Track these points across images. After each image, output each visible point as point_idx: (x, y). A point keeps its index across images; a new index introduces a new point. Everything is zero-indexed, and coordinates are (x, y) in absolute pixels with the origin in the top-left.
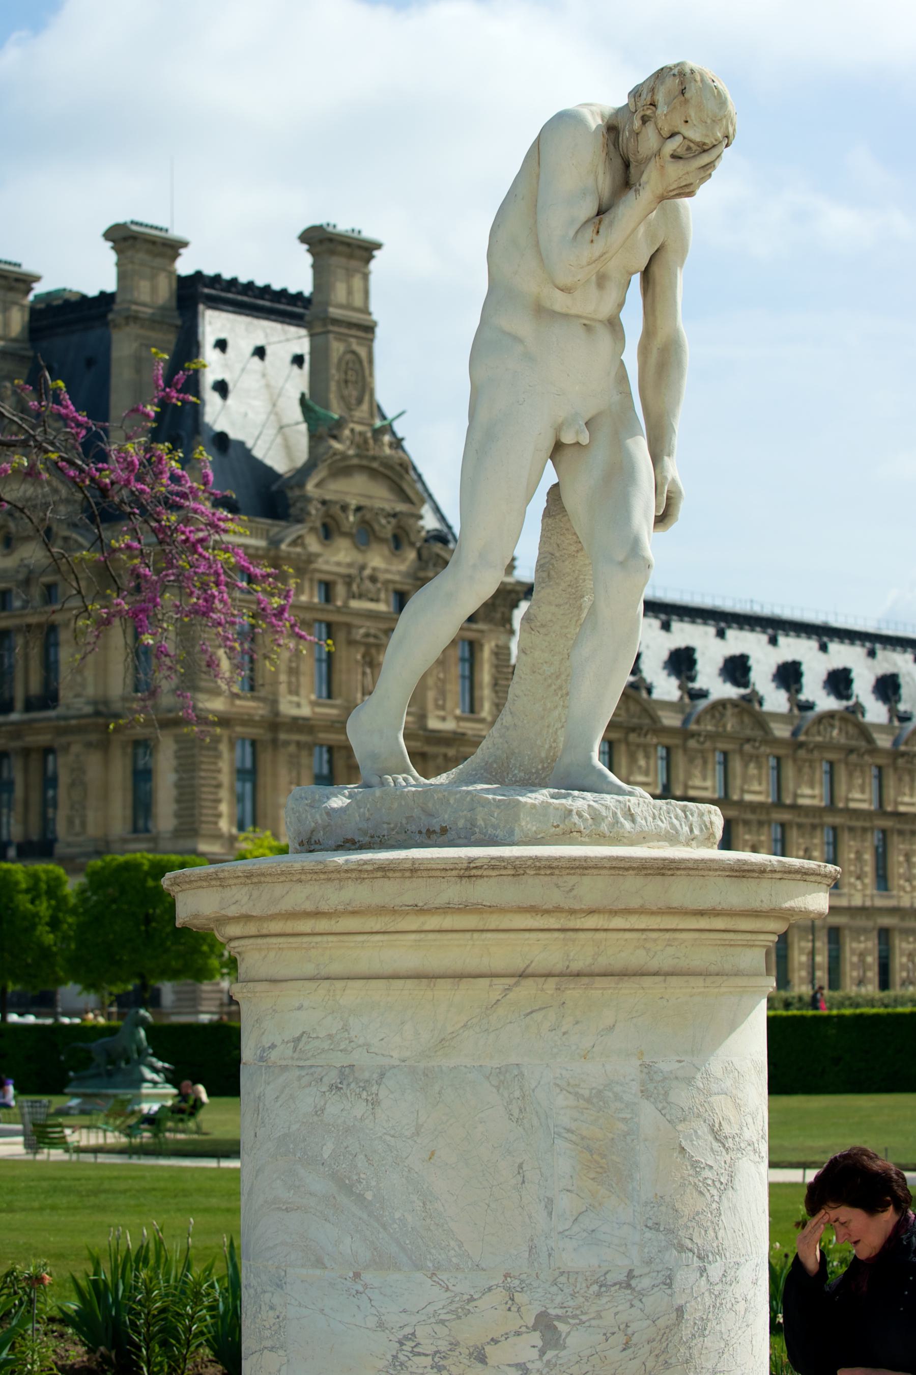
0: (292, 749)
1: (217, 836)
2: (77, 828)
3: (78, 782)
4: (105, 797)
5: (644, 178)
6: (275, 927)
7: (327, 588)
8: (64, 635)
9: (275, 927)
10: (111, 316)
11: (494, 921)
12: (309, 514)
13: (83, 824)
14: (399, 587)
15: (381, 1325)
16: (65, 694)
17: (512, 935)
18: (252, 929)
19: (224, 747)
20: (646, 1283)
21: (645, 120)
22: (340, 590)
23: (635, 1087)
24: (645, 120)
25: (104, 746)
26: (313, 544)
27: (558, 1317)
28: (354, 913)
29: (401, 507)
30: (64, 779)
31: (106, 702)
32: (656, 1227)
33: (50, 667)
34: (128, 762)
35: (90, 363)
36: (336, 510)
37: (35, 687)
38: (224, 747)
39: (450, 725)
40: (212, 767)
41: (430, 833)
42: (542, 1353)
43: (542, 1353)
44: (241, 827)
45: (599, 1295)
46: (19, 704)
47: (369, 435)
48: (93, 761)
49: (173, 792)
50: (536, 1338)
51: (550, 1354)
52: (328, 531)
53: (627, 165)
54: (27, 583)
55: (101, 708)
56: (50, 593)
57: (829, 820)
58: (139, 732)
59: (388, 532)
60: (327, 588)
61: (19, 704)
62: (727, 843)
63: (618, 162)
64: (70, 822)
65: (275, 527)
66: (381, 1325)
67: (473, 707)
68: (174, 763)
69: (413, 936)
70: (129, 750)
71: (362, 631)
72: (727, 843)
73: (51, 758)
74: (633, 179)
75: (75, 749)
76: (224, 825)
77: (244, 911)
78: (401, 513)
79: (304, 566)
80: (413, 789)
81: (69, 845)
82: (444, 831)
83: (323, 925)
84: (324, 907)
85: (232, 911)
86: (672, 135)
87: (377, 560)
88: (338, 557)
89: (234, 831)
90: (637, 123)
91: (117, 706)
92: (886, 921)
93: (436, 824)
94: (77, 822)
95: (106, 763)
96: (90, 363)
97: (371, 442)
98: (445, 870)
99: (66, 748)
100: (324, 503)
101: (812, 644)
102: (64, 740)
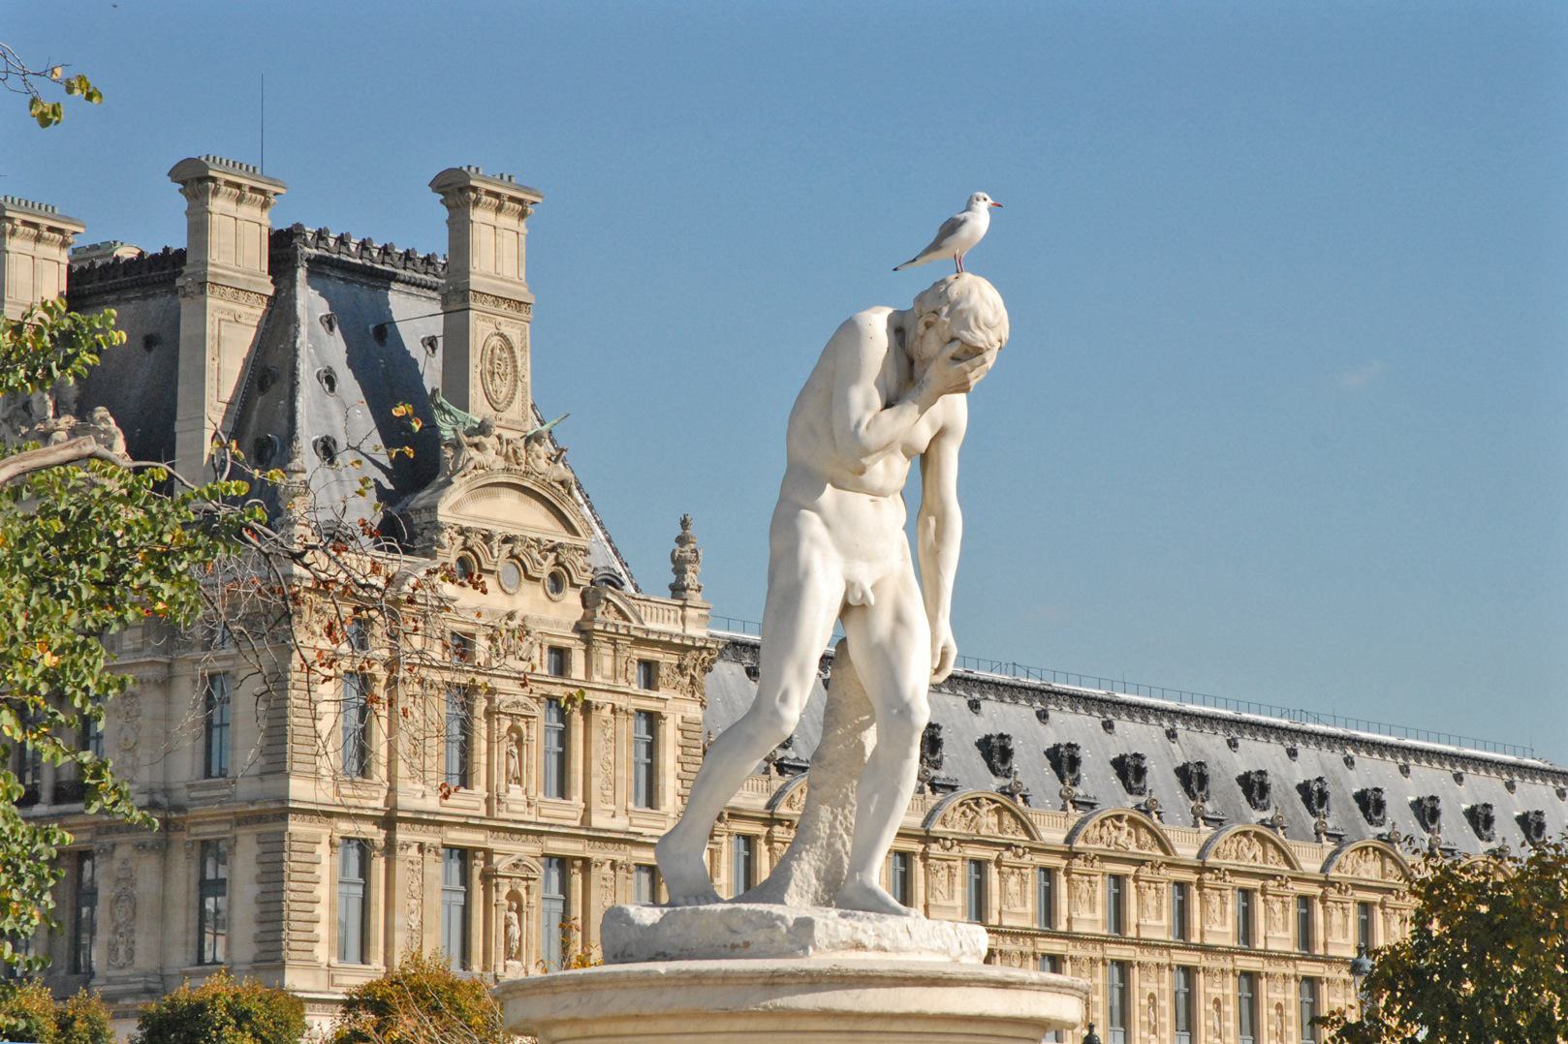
0: (413, 852)
1: (312, 965)
2: (122, 959)
3: (125, 897)
4: (163, 917)
5: (928, 375)
6: (599, 1029)
7: (463, 645)
9: (599, 1029)
10: (179, 282)
11: (791, 1025)
12: (441, 546)
13: (131, 953)
14: (556, 641)
17: (807, 1037)
18: (577, 1031)
19: (323, 851)
21: (928, 325)
22: (482, 644)
24: (928, 325)
25: (162, 848)
29: (562, 537)
30: (105, 891)
31: (167, 791)
34: (194, 870)
36: (475, 541)
39: (620, 823)
40: (307, 877)
41: (734, 946)
44: (343, 956)
46: (46, 794)
47: (521, 443)
48: (147, 869)
49: (255, 909)
52: (467, 572)
53: (911, 362)
55: (159, 798)
57: (1116, 952)
58: (209, 831)
59: (548, 566)
61: (46, 794)
63: (904, 362)
64: (112, 949)
68: (256, 870)
69: (723, 1037)
70: (196, 854)
71: (509, 700)
73: (87, 864)
74: (916, 375)
75: (121, 852)
76: (322, 953)
77: (572, 1014)
78: (561, 545)
80: (729, 906)
81: (109, 981)
82: (747, 944)
83: (642, 1027)
84: (646, 1011)
85: (561, 1015)
86: (953, 340)
87: (530, 601)
89: (334, 961)
90: (921, 328)
91: (182, 796)
93: (739, 940)
94: (122, 949)
95: (165, 873)
97: (522, 452)
98: (753, 977)
99: (109, 852)
100: (462, 532)
102: (107, 840)
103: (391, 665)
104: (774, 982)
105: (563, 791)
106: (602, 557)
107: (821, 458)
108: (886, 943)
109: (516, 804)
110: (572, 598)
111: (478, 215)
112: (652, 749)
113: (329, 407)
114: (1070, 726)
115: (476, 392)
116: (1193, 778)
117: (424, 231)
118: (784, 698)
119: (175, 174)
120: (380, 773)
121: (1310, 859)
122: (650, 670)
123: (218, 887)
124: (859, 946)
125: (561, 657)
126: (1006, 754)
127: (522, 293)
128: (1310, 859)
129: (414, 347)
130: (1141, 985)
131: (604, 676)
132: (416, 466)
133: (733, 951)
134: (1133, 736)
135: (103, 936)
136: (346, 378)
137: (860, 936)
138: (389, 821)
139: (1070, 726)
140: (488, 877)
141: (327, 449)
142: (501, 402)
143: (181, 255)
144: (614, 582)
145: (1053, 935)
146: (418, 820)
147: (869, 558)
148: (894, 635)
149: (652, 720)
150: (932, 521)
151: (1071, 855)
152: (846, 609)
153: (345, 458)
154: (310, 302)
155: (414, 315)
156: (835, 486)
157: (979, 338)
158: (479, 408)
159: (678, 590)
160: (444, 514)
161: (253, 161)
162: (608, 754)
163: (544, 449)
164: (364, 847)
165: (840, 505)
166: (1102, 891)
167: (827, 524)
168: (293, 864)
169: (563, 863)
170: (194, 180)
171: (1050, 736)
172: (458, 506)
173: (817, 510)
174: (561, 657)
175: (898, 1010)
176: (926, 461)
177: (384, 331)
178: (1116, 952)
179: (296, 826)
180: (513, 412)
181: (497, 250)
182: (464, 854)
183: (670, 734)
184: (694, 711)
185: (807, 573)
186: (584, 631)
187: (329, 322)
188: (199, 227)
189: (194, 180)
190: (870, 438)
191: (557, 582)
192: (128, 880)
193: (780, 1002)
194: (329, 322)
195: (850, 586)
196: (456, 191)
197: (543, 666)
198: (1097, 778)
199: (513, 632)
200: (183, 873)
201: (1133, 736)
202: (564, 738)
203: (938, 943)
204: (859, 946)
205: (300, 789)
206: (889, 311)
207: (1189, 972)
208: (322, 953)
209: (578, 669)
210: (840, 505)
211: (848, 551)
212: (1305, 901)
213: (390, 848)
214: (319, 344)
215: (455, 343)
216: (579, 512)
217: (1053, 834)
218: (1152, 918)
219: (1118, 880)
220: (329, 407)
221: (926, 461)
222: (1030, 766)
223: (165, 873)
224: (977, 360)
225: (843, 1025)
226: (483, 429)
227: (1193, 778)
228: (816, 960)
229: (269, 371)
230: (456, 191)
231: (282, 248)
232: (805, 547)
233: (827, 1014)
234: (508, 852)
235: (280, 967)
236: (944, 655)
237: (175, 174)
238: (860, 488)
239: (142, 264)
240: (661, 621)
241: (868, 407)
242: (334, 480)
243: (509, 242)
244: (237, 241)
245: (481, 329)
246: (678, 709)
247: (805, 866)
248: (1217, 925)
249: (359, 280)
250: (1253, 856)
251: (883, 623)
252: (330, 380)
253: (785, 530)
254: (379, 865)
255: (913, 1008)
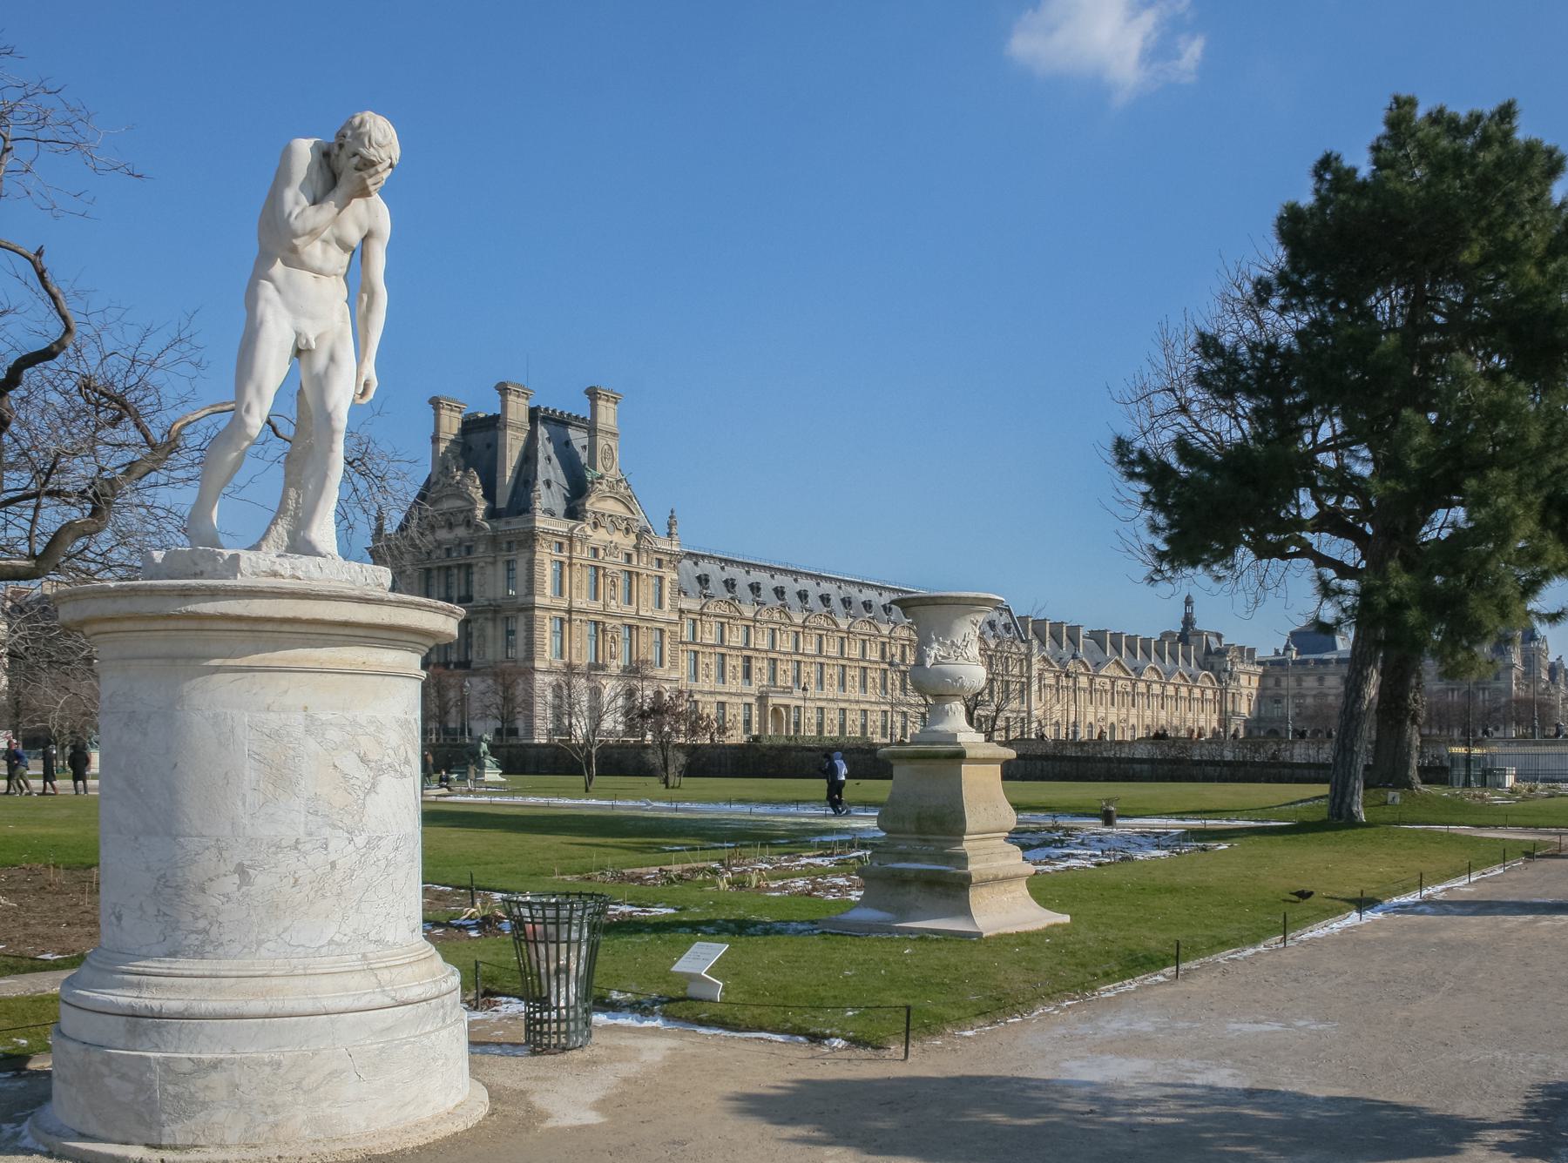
3: (482, 636)
7: (596, 551)
8: (475, 569)
15: (148, 869)
16: (476, 596)
19: (547, 621)
20: (309, 846)
22: (601, 553)
23: (302, 728)
26: (589, 531)
27: (249, 867)
28: (129, 619)
30: (475, 634)
32: (316, 813)
33: (469, 583)
35: (489, 446)
37: (463, 593)
38: (547, 621)
42: (239, 888)
43: (239, 888)
45: (276, 853)
50: (236, 878)
51: (244, 889)
54: (459, 545)
56: (469, 550)
57: (819, 660)
59: (624, 525)
60: (596, 551)
62: (393, 589)
65: (572, 523)
66: (148, 869)
67: (660, 606)
72: (393, 589)
79: (584, 540)
83: (115, 626)
86: (355, 155)
87: (618, 537)
88: (600, 536)
92: (843, 705)
96: (489, 446)
101: (813, 583)
103: (570, 558)
104: (186, 594)
105: (630, 603)
106: (643, 522)
107: (277, 242)
108: (300, 574)
109: (613, 606)
110: (633, 536)
111: (600, 402)
112: (661, 589)
113: (549, 469)
114: (805, 584)
115: (599, 464)
116: (846, 602)
117: (582, 409)
118: (248, 410)
119: (497, 388)
120: (567, 596)
121: (885, 630)
122: (660, 561)
123: (512, 632)
124: (275, 574)
125: (629, 556)
126: (783, 593)
127: (616, 430)
128: (885, 630)
129: (578, 449)
130: (827, 671)
131: (643, 564)
132: (578, 490)
133: (195, 576)
134: (826, 587)
135: (475, 649)
136: (554, 457)
137: (277, 567)
138: (569, 611)
139: (805, 584)
140: (604, 631)
141: (548, 484)
142: (607, 469)
143: (496, 418)
144: (648, 532)
145: (797, 653)
146: (579, 612)
147: (313, 317)
148: (327, 368)
149: (661, 579)
150: (365, 297)
151: (804, 627)
152: (298, 352)
153: (554, 487)
154: (542, 432)
155: (578, 438)
156: (285, 263)
157: (372, 153)
158: (600, 470)
159: (670, 534)
160: (588, 506)
161: (522, 382)
162: (646, 591)
163: (623, 484)
164: (562, 620)
165: (288, 276)
166: (815, 639)
167: (278, 290)
168: (537, 625)
169: (630, 627)
170: (503, 389)
171: (798, 587)
172: (593, 504)
173: (271, 279)
174: (629, 556)
175: (305, 617)
176: (359, 254)
177: (568, 443)
178: (819, 660)
179: (537, 612)
180: (613, 471)
181: (607, 415)
182: (596, 623)
183: (667, 584)
184: (675, 576)
185: (261, 323)
186: (637, 547)
187: (549, 439)
188: (504, 406)
189: (503, 389)
190: (297, 225)
191: (627, 531)
192: (482, 630)
193: (191, 608)
194: (549, 439)
195: (298, 335)
196: (593, 394)
197: (621, 559)
198: (814, 600)
199: (611, 548)
200: (501, 631)
201: (826, 587)
202: (630, 584)
203: (346, 576)
204: (275, 574)
205: (538, 600)
206: (312, 141)
207: (844, 667)
208: (547, 655)
209: (635, 561)
210: (288, 276)
211: (295, 310)
212: (883, 644)
213: (570, 620)
214: (545, 448)
215: (592, 448)
216: (636, 507)
217: (798, 620)
218: (832, 649)
219: (821, 636)
220: (549, 469)
221: (359, 254)
222: (791, 597)
223: (495, 627)
224: (372, 171)
225: (244, 626)
226: (602, 477)
227: (846, 602)
228: (239, 581)
229: (529, 456)
230: (593, 394)
231: (533, 414)
232: (261, 305)
233: (225, 617)
234: (611, 623)
235: (533, 660)
236: (366, 386)
237: (497, 388)
238: (302, 265)
239: (486, 418)
240: (664, 545)
241: (297, 203)
242: (548, 496)
243: (611, 413)
244: (517, 411)
245: (601, 442)
246: (670, 576)
247: (280, 528)
248: (854, 651)
249: (559, 422)
250: (866, 629)
251: (321, 361)
252: (549, 459)
253: (251, 299)
254: (566, 626)
255: (290, 615)
